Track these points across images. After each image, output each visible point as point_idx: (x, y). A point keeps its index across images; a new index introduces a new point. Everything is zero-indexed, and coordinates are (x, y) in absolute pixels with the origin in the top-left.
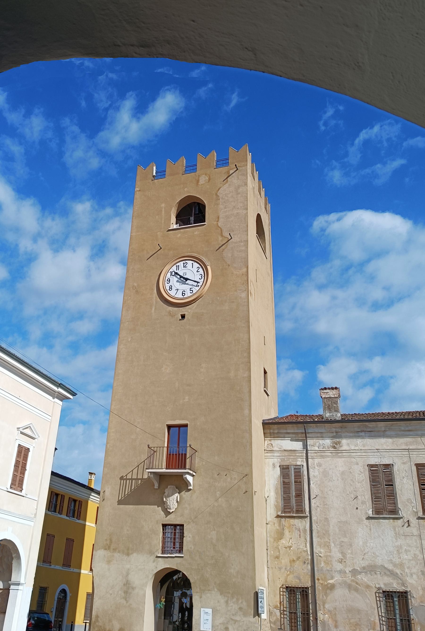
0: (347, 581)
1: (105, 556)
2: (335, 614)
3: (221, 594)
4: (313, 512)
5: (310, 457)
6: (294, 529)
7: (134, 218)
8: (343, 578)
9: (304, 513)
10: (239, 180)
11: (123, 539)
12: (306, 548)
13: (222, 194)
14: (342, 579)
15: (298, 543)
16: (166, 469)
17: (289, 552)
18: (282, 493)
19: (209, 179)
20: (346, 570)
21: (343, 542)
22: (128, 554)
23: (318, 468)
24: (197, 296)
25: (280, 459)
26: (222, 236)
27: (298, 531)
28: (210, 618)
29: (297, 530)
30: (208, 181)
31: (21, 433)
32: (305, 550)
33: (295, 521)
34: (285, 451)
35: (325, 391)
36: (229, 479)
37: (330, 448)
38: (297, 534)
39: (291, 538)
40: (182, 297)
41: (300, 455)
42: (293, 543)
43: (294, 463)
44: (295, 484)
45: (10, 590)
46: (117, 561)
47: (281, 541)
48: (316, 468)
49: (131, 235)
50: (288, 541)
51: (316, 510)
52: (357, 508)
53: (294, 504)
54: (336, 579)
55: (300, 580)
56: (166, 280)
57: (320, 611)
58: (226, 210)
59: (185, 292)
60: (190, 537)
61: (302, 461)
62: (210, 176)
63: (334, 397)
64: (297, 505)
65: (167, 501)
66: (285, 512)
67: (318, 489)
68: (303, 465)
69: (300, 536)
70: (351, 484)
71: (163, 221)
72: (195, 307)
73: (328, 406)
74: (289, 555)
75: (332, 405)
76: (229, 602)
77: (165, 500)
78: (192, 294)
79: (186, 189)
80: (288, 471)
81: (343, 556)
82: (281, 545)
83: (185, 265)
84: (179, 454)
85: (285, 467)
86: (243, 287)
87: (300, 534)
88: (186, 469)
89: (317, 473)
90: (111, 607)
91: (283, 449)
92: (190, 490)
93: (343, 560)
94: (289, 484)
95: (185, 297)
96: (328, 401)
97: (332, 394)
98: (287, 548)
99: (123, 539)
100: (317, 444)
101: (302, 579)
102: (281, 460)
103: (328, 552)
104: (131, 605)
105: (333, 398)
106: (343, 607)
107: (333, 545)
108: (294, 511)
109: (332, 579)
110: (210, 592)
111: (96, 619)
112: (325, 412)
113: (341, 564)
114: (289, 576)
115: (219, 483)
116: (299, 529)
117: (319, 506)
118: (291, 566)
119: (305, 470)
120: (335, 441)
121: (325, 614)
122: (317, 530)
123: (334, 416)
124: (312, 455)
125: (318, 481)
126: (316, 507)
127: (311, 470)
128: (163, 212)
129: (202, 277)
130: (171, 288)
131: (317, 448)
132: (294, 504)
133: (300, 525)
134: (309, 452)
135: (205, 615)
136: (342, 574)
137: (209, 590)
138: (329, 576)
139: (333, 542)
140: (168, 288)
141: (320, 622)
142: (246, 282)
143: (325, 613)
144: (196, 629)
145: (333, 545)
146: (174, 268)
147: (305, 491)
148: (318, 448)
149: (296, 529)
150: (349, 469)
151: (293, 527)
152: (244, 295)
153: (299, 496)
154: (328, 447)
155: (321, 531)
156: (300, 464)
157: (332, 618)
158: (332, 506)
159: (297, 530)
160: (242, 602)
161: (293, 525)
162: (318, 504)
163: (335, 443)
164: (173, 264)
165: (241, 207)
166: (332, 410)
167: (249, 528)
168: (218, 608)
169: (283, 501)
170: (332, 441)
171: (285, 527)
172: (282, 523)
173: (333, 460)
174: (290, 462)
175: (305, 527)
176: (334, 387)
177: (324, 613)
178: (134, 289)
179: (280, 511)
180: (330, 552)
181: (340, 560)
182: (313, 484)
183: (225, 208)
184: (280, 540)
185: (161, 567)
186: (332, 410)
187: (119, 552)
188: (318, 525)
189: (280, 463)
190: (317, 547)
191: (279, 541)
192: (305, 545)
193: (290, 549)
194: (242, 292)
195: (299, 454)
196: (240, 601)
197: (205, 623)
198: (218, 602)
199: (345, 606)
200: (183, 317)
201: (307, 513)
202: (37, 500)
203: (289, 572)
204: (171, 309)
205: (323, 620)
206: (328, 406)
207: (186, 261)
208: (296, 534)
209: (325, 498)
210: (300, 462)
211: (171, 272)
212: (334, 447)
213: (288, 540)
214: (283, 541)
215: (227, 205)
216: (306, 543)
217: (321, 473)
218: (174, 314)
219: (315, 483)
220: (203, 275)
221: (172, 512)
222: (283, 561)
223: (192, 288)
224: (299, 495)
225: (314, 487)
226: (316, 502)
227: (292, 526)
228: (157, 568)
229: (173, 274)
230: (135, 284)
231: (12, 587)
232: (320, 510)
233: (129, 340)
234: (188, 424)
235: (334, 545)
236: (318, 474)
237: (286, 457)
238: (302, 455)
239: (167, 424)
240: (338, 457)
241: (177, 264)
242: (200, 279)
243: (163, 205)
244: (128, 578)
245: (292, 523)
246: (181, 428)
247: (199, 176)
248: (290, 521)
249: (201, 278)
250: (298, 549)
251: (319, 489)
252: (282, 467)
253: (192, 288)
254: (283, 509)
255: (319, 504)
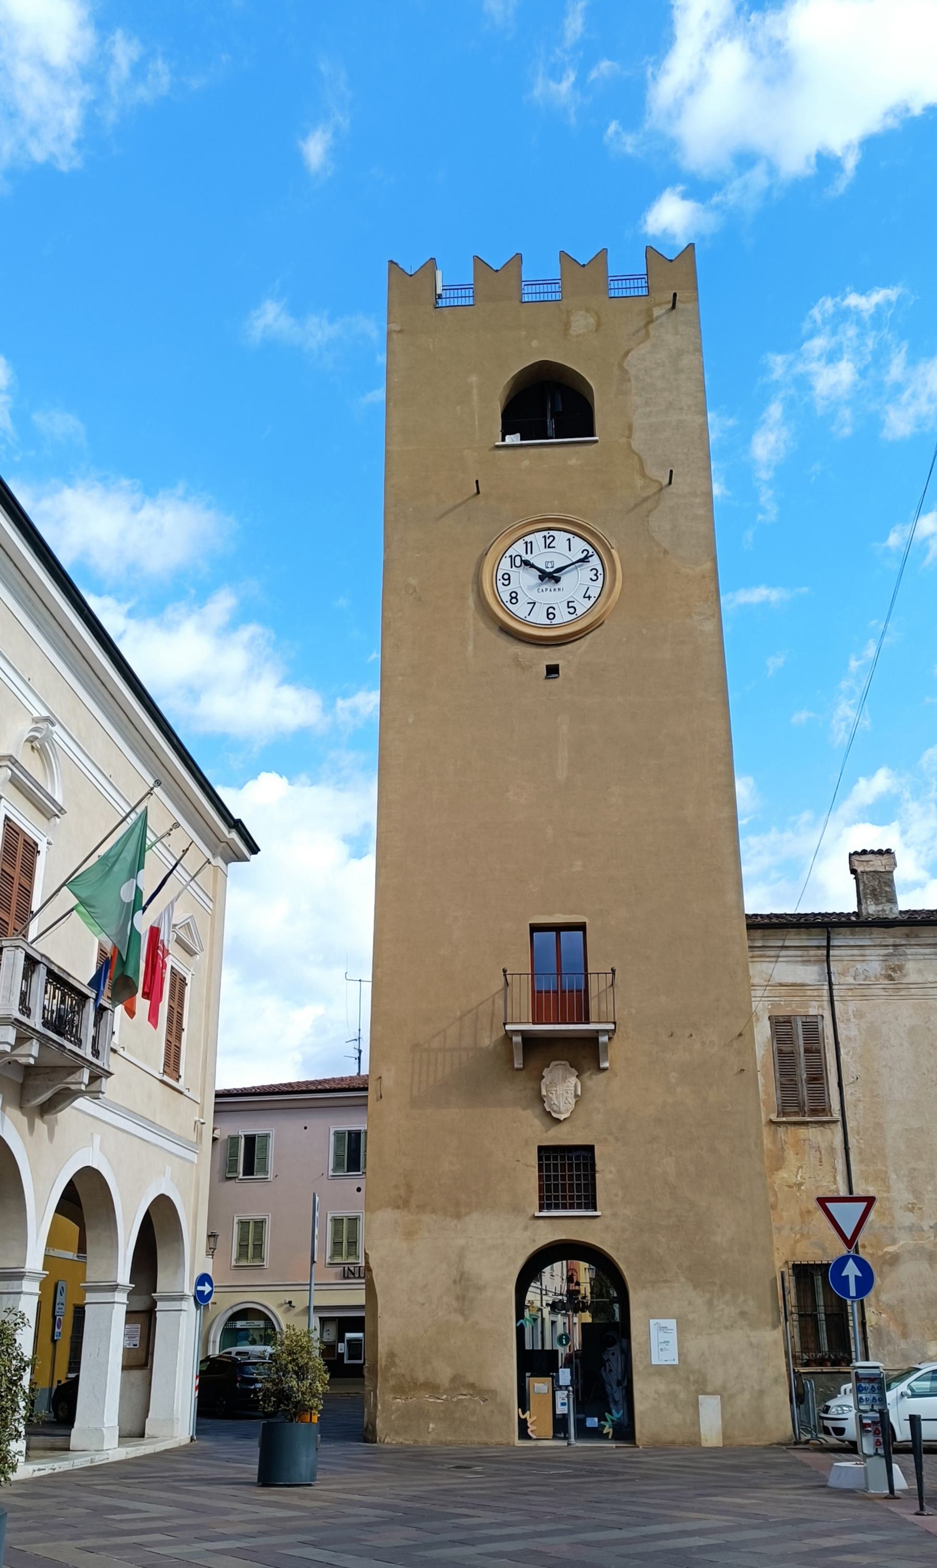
0: (925, 1246)
1: (396, 1222)
2: (903, 1311)
3: (695, 1287)
4: (848, 1113)
5: (838, 998)
6: (807, 1148)
7: (391, 404)
8: (916, 1240)
9: (829, 1114)
10: (679, 336)
11: (442, 1182)
12: (835, 1184)
13: (635, 366)
14: (915, 1242)
15: (817, 1176)
16: (534, 1023)
17: (798, 1194)
18: (778, 1075)
19: (599, 325)
20: (922, 1224)
21: (914, 1169)
22: (458, 1216)
23: (856, 1021)
24: (589, 623)
25: (769, 1003)
26: (643, 475)
27: (816, 1151)
28: (673, 1337)
29: (814, 1150)
30: (594, 329)
31: (176, 941)
32: (832, 1190)
33: (808, 1132)
34: (781, 985)
35: (864, 858)
36: (697, 1046)
37: (881, 980)
38: (814, 1157)
39: (801, 1167)
40: (548, 622)
41: (815, 994)
42: (806, 1176)
43: (802, 1011)
44: (807, 1055)
45: (157, 1313)
46: (429, 1231)
47: (777, 1174)
48: (852, 1020)
49: (387, 451)
50: (795, 1173)
51: (855, 1107)
52: (306, 1128)
53: (806, 1097)
54: (902, 1243)
55: (824, 1250)
56: (499, 576)
57: (870, 1307)
58: (648, 409)
59: (554, 609)
60: (611, 1172)
61: (817, 1008)
62: (598, 317)
63: (884, 870)
64: (812, 1099)
65: (551, 1095)
66: (785, 1114)
67: (859, 1065)
68: (822, 1016)
69: (821, 1162)
70: (930, 1054)
71: (477, 423)
72: (583, 649)
73: (871, 891)
74: (797, 1201)
75: (880, 888)
76: (716, 1302)
77: (545, 1094)
78: (574, 616)
79: (535, 343)
80: (790, 1027)
81: (916, 1198)
82: (778, 1182)
83: (548, 541)
84: (563, 992)
85: (781, 1019)
86: (706, 606)
87: (821, 1158)
88: (588, 1023)
89: (854, 1032)
90: (426, 1331)
91: (774, 982)
92: (605, 1069)
93: (915, 1206)
94: (792, 1055)
95: (554, 622)
96: (871, 879)
97: (880, 864)
98: (793, 1187)
99: (442, 1182)
100: (852, 971)
101: (827, 1248)
102: (771, 1004)
103: (884, 1191)
104: (477, 1323)
105: (883, 874)
106: (919, 1297)
107: (894, 1176)
108: (806, 1111)
109: (894, 1245)
110: (668, 1284)
111: (389, 1360)
112: (867, 903)
113: (911, 1214)
114: (799, 1244)
115: (673, 1054)
116: (819, 1147)
117: (861, 1099)
118: (803, 1222)
119: (828, 1027)
120: (891, 964)
121: (880, 1313)
122: (860, 1148)
123: (887, 912)
124: (842, 994)
125: (859, 1049)
126: (856, 1101)
127: (840, 1025)
128: (475, 398)
129: (598, 574)
130: (512, 598)
131: (850, 980)
132: (806, 1097)
133: (819, 1138)
134: (834, 987)
135: (661, 1334)
136: (914, 1233)
137: (666, 1281)
138: (887, 1238)
139: (895, 1171)
140: (506, 598)
141: (871, 1328)
142: (712, 596)
143: (880, 1311)
144: (640, 1362)
145: (894, 1176)
146: (519, 548)
147: (830, 1070)
148: (855, 979)
149: (811, 1147)
150: (926, 1023)
151: (804, 1145)
152: (709, 627)
153: (816, 1079)
154: (875, 977)
155: (867, 1150)
156: (816, 1014)
157: (896, 1320)
158: (889, 1099)
159: (814, 1150)
160: (745, 1301)
161: (804, 1141)
162: (859, 1095)
163: (890, 969)
164: (516, 536)
165: (689, 407)
166: (880, 898)
167: (753, 1147)
168: (691, 1317)
169: (779, 1092)
170: (883, 964)
171: (787, 1146)
172: (779, 1136)
173: (889, 1004)
174: (792, 1009)
175: (832, 1143)
176: (869, 850)
177: (877, 1310)
178: (412, 594)
179: (773, 1113)
180: (888, 1191)
181: (910, 1206)
182: (847, 1054)
183: (647, 404)
184: (775, 1172)
185: (546, 1238)
186: (880, 898)
187: (434, 1211)
188: (861, 1139)
189: (770, 1011)
190: (860, 1182)
191: (774, 1174)
192: (833, 1179)
193: (799, 1189)
194: (704, 619)
195: (814, 993)
196: (741, 1299)
197: (661, 1349)
198: (690, 1303)
199: (922, 1295)
200: (553, 670)
201: (834, 1115)
202: (199, 1102)
203: (798, 1236)
204: (519, 650)
205: (876, 1324)
206: (871, 891)
207: (552, 533)
208: (812, 1159)
209: (875, 1082)
210: (816, 1010)
211: (511, 556)
212: (890, 978)
213: (795, 1170)
214: (783, 1174)
215: (651, 399)
216: (835, 1175)
217: (863, 1032)
218: (527, 663)
219: (851, 1053)
220: (600, 571)
221: (564, 1119)
222: (785, 1214)
223: (573, 602)
224: (817, 1078)
225: (849, 1060)
226: (855, 1091)
227: (802, 1141)
228: (534, 1241)
229: (518, 562)
230: (413, 581)
231: (160, 1305)
232: (864, 1107)
233: (411, 720)
234: (585, 923)
235: (896, 1177)
236: (857, 1033)
237: (783, 999)
238: (820, 994)
239: (530, 922)
240: (900, 998)
241: (528, 539)
242: (591, 579)
243: (474, 379)
244: (463, 1267)
245: (802, 1137)
246: (561, 933)
247: (569, 312)
248: (797, 1131)
249: (595, 578)
250: (817, 1188)
251: (861, 1065)
252: (775, 1019)
253: (573, 602)
254: (780, 1108)
255: (861, 1095)
